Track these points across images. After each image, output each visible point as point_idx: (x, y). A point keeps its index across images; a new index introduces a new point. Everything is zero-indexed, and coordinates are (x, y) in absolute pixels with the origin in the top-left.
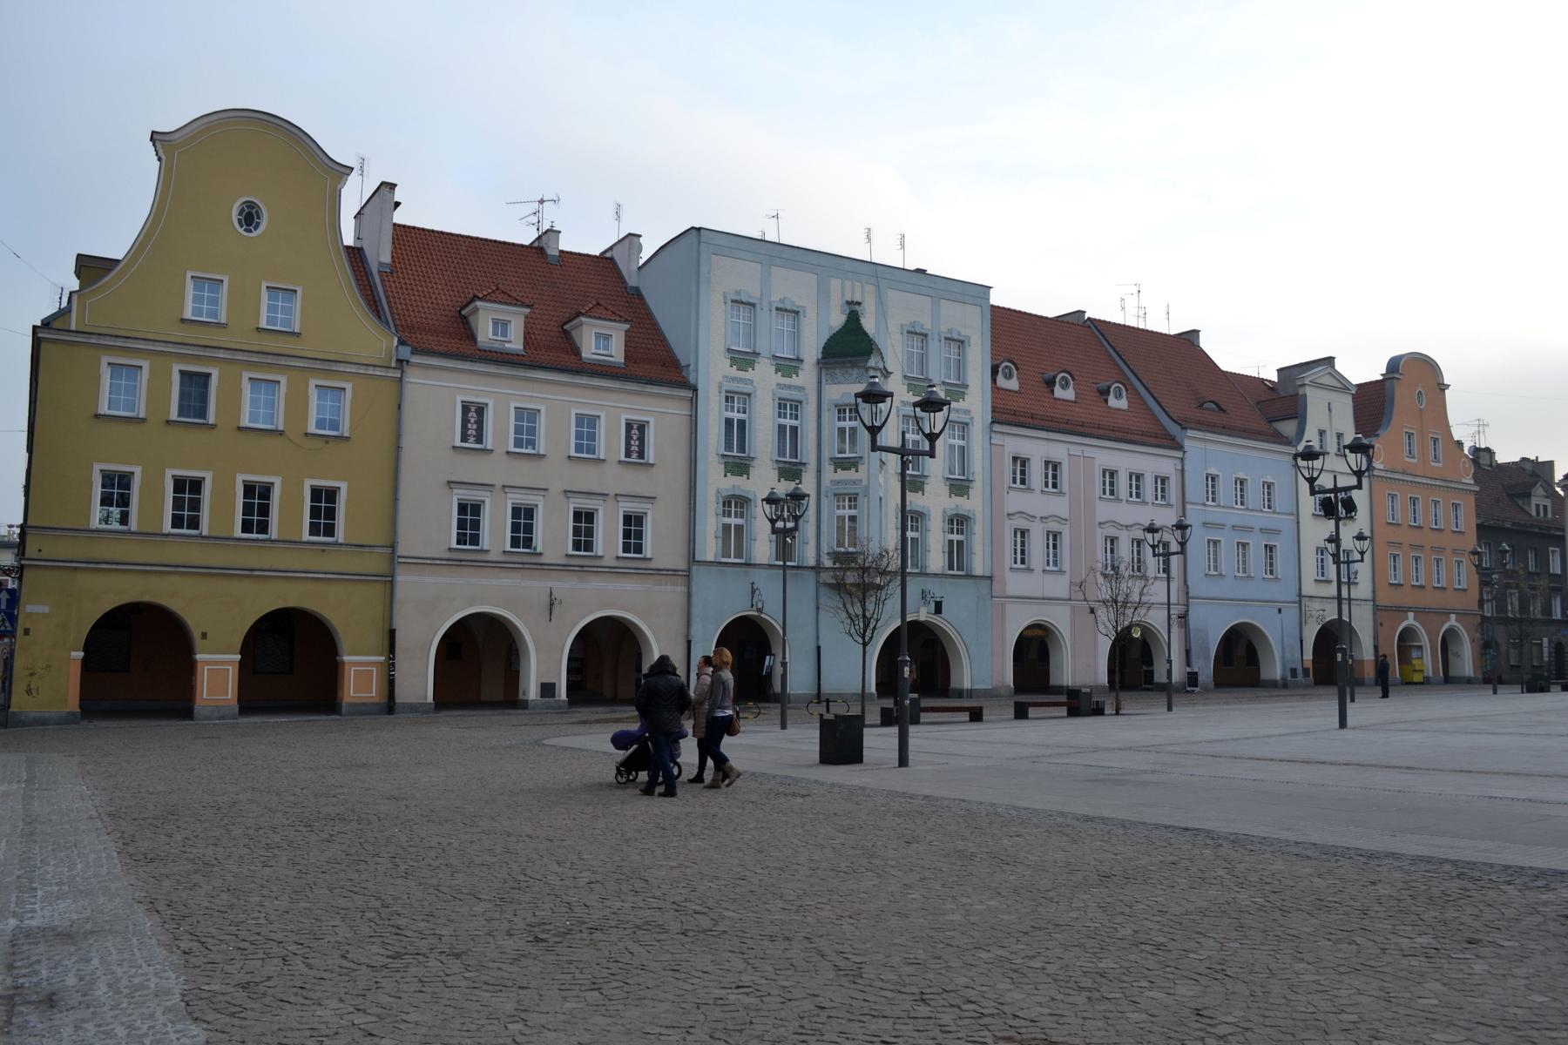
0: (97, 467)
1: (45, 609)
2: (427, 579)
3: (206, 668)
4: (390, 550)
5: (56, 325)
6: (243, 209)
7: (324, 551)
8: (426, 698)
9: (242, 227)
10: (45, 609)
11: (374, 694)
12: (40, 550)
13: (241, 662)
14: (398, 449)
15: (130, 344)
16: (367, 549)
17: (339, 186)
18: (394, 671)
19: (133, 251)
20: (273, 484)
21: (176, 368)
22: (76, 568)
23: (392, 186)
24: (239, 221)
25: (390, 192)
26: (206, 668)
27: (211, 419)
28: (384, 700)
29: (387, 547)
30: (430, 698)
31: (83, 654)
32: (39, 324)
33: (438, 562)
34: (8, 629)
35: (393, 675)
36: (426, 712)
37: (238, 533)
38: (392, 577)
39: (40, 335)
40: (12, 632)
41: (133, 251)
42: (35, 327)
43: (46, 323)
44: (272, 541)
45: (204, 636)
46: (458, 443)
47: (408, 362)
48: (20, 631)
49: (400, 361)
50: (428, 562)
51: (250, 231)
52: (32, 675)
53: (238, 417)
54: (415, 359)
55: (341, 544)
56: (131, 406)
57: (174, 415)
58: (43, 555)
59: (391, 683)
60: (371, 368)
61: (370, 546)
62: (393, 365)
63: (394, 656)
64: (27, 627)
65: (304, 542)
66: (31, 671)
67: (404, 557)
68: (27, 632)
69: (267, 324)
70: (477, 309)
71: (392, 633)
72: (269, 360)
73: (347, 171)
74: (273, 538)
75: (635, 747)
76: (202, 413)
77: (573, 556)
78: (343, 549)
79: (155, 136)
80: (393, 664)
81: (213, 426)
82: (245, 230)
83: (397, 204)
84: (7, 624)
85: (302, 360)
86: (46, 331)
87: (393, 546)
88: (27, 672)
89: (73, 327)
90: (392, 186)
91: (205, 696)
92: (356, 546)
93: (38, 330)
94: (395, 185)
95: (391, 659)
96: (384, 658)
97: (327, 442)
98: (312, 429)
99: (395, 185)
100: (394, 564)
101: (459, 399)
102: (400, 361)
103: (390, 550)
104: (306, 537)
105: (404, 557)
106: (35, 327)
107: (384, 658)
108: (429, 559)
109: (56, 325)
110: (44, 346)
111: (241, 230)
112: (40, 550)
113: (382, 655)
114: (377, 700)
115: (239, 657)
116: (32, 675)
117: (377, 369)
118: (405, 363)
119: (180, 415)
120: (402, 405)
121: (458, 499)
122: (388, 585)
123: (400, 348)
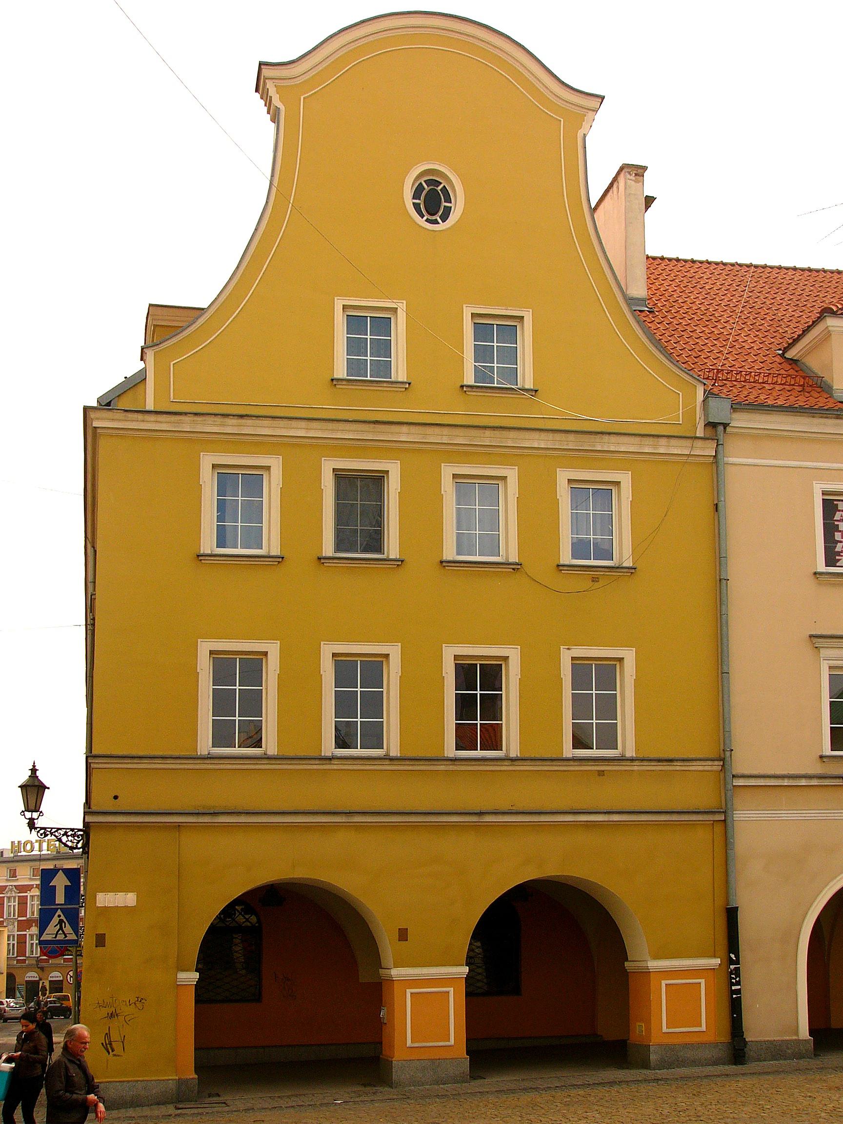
0: (205, 647)
1: (129, 899)
2: (784, 815)
3: (409, 991)
4: (716, 766)
5: (124, 403)
6: (420, 189)
7: (601, 773)
8: (796, 1032)
9: (422, 216)
10: (129, 899)
11: (704, 1028)
12: (116, 797)
13: (469, 979)
14: (721, 582)
15: (249, 428)
16: (678, 767)
17: (580, 134)
18: (738, 983)
19: (245, 264)
20: (506, 659)
21: (328, 467)
22: (179, 827)
23: (639, 171)
24: (417, 207)
25: (636, 181)
26: (409, 991)
27: (393, 547)
28: (724, 1038)
29: (712, 760)
30: (804, 1031)
31: (197, 975)
32: (95, 404)
33: (803, 782)
34: (69, 937)
35: (738, 992)
36: (800, 1056)
37: (450, 751)
38: (725, 812)
39: (96, 424)
40: (75, 942)
41: (245, 264)
42: (86, 409)
43: (107, 403)
44: (392, 759)
45: (403, 935)
46: (821, 567)
47: (725, 425)
48: (87, 942)
49: (712, 425)
50: (786, 782)
51: (435, 222)
52: (112, 1016)
53: (439, 545)
54: (741, 421)
55: (632, 760)
56: (254, 537)
57: (328, 548)
58: (123, 804)
59: (735, 1006)
60: (663, 441)
61: (683, 760)
62: (700, 433)
63: (737, 956)
64: (100, 931)
65: (568, 760)
66: (111, 1010)
67: (743, 776)
68: (100, 940)
69: (475, 382)
70: (827, 335)
71: (732, 915)
72: (487, 438)
73: (592, 103)
74: (513, 754)
75: (734, 959)
76: (375, 542)
77: (574, 759)
78: (636, 767)
79: (266, 72)
80: (737, 972)
81: (400, 562)
82: (427, 220)
83: (649, 201)
84: (68, 929)
85: (543, 435)
86: (110, 414)
87: (723, 759)
88: (104, 1012)
89: (150, 406)
90: (639, 171)
91: (409, 1043)
92: (659, 760)
93: (92, 415)
94: (645, 168)
95: (731, 962)
96: (718, 961)
97: (595, 580)
98: (566, 558)
99: (645, 168)
100: (726, 790)
101: (818, 489)
102: (712, 425)
103: (716, 766)
104: (450, 751)
105: (743, 776)
106: (86, 409)
107: (718, 961)
108: (783, 777)
109: (124, 403)
110: (104, 445)
111: (422, 222)
112: (116, 797)
113: (715, 957)
114: (710, 1038)
115: (466, 969)
116: (112, 1016)
117: (673, 442)
118: (721, 428)
119: (338, 548)
120: (720, 505)
121: (830, 668)
122: (719, 828)
123: (712, 402)
